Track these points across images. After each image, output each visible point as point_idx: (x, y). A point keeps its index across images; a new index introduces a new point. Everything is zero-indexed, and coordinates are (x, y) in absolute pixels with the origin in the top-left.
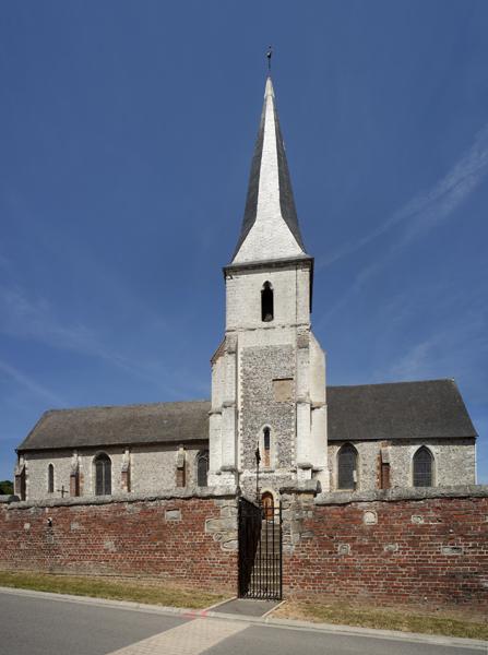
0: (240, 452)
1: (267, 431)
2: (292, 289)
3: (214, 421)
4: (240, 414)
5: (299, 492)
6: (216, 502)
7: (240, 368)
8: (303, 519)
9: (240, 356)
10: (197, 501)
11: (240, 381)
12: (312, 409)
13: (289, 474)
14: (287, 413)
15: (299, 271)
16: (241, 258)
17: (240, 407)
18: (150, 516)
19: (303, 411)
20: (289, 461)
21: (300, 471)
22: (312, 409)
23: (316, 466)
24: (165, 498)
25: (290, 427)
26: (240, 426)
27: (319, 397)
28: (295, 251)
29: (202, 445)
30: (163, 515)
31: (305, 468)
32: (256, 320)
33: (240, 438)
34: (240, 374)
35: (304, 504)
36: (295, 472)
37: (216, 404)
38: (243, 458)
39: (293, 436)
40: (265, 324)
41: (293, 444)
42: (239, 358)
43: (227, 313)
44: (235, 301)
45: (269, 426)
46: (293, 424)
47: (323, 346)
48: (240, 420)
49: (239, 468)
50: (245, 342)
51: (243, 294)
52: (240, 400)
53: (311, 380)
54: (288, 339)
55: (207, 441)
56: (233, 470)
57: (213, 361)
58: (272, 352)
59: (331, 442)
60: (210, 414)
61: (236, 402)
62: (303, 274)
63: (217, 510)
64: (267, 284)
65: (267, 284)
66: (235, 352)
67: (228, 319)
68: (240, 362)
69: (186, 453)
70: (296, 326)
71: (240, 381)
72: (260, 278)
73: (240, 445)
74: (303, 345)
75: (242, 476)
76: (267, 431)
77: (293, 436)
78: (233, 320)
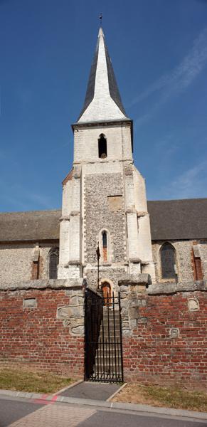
0: (84, 250)
1: (104, 234)
2: (119, 139)
3: (64, 226)
4: (84, 221)
5: (134, 284)
6: (66, 292)
7: (83, 188)
8: (138, 307)
9: (83, 180)
10: (51, 291)
11: (84, 197)
12: (138, 217)
13: (123, 267)
14: (119, 219)
15: (124, 128)
16: (83, 120)
17: (83, 215)
18: (10, 304)
19: (132, 219)
20: (123, 256)
21: (131, 265)
22: (138, 217)
23: (144, 260)
24: (24, 289)
25: (122, 230)
26: (84, 230)
27: (142, 208)
28: (120, 116)
29: (54, 244)
30: (22, 303)
31: (136, 262)
32: (95, 156)
33: (84, 239)
34: (83, 192)
35: (138, 294)
36: (128, 265)
37: (66, 212)
38: (86, 254)
39: (125, 237)
40: (101, 160)
41: (125, 243)
42: (83, 181)
43: (75, 152)
44: (80, 145)
45: (107, 230)
46: (124, 228)
47: (143, 174)
48: (84, 225)
49: (83, 262)
50: (86, 171)
51: (85, 143)
52: (84, 210)
53: (136, 196)
54: (118, 169)
55: (57, 241)
56: (78, 264)
57: (64, 183)
58: (107, 178)
59: (154, 242)
60: (61, 220)
61: (81, 212)
62: (126, 130)
63: (67, 300)
64: (102, 135)
65: (102, 135)
66: (80, 177)
67: (75, 156)
68: (83, 184)
69: (41, 250)
70: (123, 161)
71: (84, 197)
72: (97, 132)
73: (84, 244)
74: (128, 173)
75: (85, 269)
76: (104, 234)
77: (125, 237)
78: (78, 156)
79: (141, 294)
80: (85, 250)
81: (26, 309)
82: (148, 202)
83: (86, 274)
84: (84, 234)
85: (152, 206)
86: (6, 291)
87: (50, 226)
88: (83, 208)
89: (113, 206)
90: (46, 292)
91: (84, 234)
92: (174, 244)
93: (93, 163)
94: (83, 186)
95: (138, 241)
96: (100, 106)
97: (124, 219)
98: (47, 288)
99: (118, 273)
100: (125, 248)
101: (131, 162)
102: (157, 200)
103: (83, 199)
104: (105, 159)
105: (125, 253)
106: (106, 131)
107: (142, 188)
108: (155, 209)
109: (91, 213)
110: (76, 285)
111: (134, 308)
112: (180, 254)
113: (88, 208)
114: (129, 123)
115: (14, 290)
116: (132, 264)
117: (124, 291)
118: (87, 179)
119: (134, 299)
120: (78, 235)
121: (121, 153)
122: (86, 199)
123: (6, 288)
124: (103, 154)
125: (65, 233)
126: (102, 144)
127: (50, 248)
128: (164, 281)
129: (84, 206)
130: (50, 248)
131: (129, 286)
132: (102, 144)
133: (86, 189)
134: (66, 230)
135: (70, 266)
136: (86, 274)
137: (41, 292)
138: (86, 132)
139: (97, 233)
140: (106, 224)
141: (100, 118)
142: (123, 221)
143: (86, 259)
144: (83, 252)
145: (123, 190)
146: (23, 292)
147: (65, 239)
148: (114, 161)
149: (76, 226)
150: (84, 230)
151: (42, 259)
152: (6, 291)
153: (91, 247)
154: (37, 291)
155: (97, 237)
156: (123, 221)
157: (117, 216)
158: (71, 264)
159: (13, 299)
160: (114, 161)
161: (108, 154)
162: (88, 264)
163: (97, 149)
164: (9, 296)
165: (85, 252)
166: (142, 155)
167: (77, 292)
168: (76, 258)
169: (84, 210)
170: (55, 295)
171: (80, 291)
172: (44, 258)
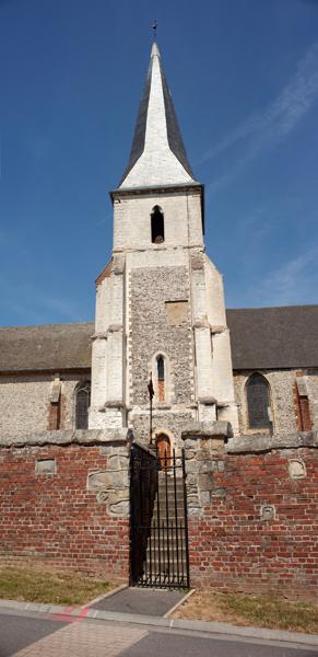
0: (129, 384)
1: (160, 360)
2: (183, 215)
3: (98, 347)
4: (129, 339)
5: (205, 437)
6: (102, 449)
7: (128, 290)
8: (212, 473)
9: (128, 277)
10: (78, 448)
11: (128, 302)
12: (212, 334)
13: (189, 411)
14: (184, 336)
15: (190, 197)
16: (128, 184)
17: (128, 331)
18: (15, 468)
19: (202, 336)
20: (188, 395)
21: (201, 407)
22: (212, 334)
23: (221, 400)
24: (36, 444)
25: (187, 354)
26: (129, 354)
27: (218, 320)
28: (184, 178)
29: (83, 375)
30: (33, 466)
31: (208, 404)
32: (146, 240)
33: (129, 367)
34: (128, 295)
35: (212, 453)
36: (196, 408)
37: (101, 326)
38: (132, 391)
39: (191, 365)
40: (155, 246)
41: (191, 374)
42: (127, 279)
43: (115, 234)
44: (124, 223)
45: (164, 354)
46: (191, 351)
47: (220, 268)
48: (129, 346)
49: (127, 404)
50: (133, 263)
51: (131, 219)
52: (128, 324)
53: (208, 301)
54: (181, 260)
55: (88, 371)
56: (120, 407)
57: (98, 281)
58: (164, 274)
59: (237, 372)
60: (94, 339)
61: (124, 327)
62: (194, 200)
63: (103, 461)
64: (157, 208)
65: (157, 208)
66: (123, 273)
67: (115, 239)
68: (128, 283)
69: (63, 384)
70: (189, 248)
71: (128, 302)
72: (150, 203)
73: (129, 376)
74: (197, 266)
75: (131, 414)
76: (160, 360)
77: (191, 365)
78: (119, 241)
79: (216, 453)
80: (131, 384)
81: (39, 476)
82: (227, 311)
83: (133, 422)
84: (129, 360)
85: (233, 317)
86: (9, 447)
87: (76, 348)
88: (127, 319)
89: (174, 317)
90: (71, 449)
91: (129, 360)
92: (267, 376)
93: (143, 251)
94: (127, 286)
95: (213, 371)
96: (153, 164)
97: (190, 336)
98: (73, 442)
99: (182, 420)
100: (192, 382)
101: (202, 249)
102: (242, 307)
103: (127, 306)
104: (161, 245)
105: (192, 389)
106: (163, 202)
107: (218, 289)
108: (238, 322)
109: (140, 327)
110: (117, 439)
111: (205, 473)
112: (277, 391)
113: (135, 320)
114: (199, 190)
115: (22, 447)
116: (203, 406)
117: (190, 448)
118: (134, 275)
119: (206, 460)
120: (120, 361)
121: (186, 235)
122: (132, 306)
123: (10, 443)
124: (159, 238)
125: (100, 358)
126: (157, 222)
127: (77, 382)
128: (252, 432)
129: (128, 316)
130: (77, 382)
131: (199, 440)
132: (157, 222)
133: (133, 291)
134: (101, 354)
135: (107, 409)
136: (133, 422)
137: (63, 449)
138: (132, 203)
139: (148, 358)
140: (162, 345)
141: (154, 182)
142: (189, 340)
143: (132, 399)
144: (127, 387)
145: (189, 293)
146: (35, 450)
147: (100, 368)
148: (175, 248)
149: (116, 348)
150: (129, 354)
151: (65, 399)
152: (9, 447)
153: (139, 380)
154: (56, 448)
155: (149, 364)
156: (189, 340)
157: (179, 333)
158: (110, 406)
159: (20, 460)
160: (175, 248)
161: (165, 237)
162: (136, 407)
163: (149, 228)
164: (13, 456)
165: (131, 387)
166: (218, 239)
167: (119, 450)
168: (117, 396)
169: (128, 324)
170: (85, 454)
171: (122, 448)
172: (68, 397)
